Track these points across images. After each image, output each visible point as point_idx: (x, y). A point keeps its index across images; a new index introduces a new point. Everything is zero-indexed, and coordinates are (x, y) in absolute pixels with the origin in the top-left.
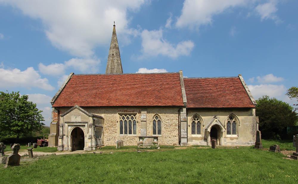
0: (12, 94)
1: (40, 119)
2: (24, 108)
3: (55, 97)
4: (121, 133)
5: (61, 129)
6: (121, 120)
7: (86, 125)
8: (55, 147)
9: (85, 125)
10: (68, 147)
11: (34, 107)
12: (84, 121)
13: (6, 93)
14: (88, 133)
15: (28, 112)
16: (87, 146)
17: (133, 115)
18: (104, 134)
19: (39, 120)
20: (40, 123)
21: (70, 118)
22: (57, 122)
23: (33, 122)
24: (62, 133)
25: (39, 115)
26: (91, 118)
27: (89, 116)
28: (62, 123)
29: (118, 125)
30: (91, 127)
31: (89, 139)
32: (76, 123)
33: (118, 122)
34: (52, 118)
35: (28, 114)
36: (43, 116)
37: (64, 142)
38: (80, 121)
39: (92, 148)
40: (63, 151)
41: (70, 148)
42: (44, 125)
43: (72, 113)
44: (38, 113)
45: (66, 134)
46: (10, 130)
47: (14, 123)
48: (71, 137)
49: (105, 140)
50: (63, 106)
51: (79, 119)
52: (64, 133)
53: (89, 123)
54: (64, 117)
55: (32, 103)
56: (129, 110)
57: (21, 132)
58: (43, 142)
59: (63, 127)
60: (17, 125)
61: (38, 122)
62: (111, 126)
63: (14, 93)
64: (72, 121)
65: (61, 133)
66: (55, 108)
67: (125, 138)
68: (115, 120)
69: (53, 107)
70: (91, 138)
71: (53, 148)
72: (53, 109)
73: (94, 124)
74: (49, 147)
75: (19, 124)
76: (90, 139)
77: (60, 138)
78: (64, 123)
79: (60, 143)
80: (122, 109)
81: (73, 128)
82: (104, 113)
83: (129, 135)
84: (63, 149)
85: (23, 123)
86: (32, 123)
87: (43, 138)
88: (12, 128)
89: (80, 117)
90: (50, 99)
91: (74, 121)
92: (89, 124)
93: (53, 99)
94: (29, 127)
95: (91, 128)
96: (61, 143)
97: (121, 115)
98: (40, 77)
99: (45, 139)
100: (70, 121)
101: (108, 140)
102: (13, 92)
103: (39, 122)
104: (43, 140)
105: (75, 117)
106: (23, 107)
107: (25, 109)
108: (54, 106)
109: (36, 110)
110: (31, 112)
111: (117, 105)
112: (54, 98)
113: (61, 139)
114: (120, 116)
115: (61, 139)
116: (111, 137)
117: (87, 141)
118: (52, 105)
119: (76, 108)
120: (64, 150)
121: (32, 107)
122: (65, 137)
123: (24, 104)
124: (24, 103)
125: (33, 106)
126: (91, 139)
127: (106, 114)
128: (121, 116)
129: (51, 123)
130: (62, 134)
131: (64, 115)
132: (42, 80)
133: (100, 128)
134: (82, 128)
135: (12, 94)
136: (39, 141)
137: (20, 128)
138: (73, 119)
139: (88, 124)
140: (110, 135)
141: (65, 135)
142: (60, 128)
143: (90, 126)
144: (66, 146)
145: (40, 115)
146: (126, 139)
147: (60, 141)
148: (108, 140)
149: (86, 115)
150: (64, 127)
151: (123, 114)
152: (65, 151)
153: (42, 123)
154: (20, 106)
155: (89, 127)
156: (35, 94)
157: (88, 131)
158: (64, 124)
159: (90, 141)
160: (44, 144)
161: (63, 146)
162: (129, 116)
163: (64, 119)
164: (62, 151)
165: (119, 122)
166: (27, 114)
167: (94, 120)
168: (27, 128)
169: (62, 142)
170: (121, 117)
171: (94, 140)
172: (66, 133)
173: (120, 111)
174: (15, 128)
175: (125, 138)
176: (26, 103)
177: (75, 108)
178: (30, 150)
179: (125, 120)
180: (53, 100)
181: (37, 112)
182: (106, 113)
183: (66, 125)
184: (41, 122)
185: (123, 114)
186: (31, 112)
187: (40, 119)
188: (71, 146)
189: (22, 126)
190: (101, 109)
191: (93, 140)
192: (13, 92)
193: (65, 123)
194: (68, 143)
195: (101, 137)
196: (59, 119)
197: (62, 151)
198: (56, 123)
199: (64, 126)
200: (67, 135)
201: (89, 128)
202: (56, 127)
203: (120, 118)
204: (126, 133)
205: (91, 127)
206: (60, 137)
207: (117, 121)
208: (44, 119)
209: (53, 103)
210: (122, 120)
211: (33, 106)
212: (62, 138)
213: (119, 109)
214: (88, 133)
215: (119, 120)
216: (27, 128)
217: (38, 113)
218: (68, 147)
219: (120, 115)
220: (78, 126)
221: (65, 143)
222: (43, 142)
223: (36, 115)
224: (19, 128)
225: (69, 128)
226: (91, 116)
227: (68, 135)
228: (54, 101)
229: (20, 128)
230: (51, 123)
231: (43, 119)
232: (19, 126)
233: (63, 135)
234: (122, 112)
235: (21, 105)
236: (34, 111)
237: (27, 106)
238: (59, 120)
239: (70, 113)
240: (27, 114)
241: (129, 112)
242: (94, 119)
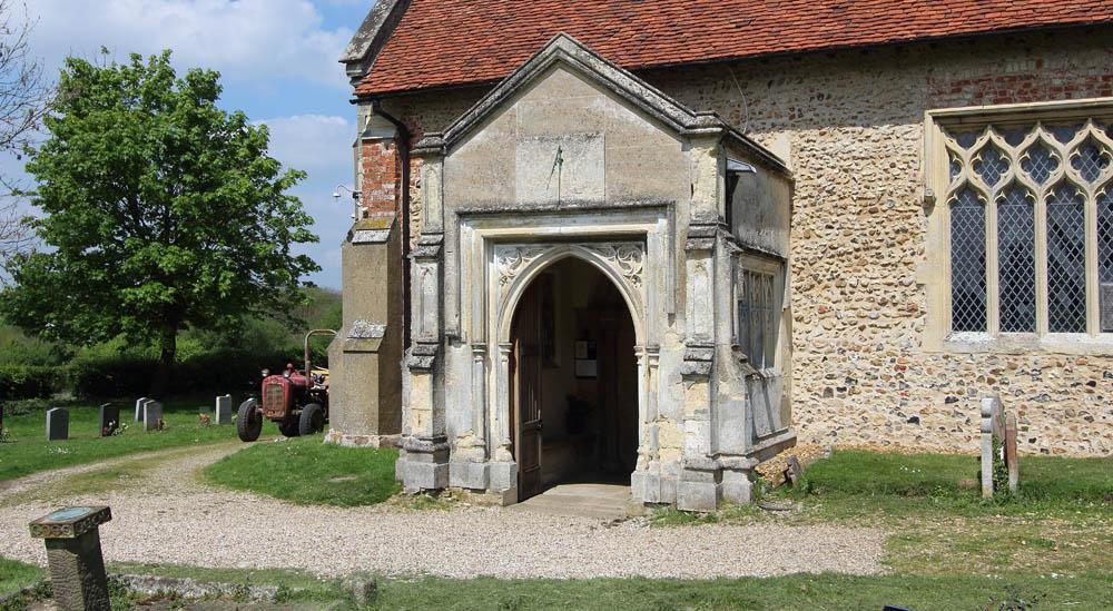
0: (131, 68)
1: (293, 230)
2: (197, 154)
3: (374, 14)
4: (967, 314)
5: (423, 278)
6: (967, 189)
7: (656, 229)
8: (376, 443)
9: (642, 237)
10: (488, 455)
11: (254, 151)
12: (637, 191)
13: (100, 63)
14: (671, 317)
15: (220, 184)
16: (669, 458)
17: (1098, 123)
18: (790, 331)
19: (285, 238)
20: (289, 259)
21: (505, 173)
22: (394, 225)
23: (250, 252)
24: (431, 317)
25: (282, 205)
26: (704, 164)
27: (689, 138)
28: (435, 217)
29: (939, 226)
30: (712, 252)
31: (689, 377)
32: (563, 212)
33: (929, 204)
34: (355, 196)
35: (220, 191)
36: (308, 208)
37: (449, 402)
38: (595, 195)
39: (718, 473)
40: (443, 498)
41: (504, 466)
42: (313, 277)
43: (519, 121)
44: (278, 187)
45: (465, 328)
46: (117, 308)
47: (140, 255)
48: (511, 356)
49: (796, 392)
50: (439, 79)
51: (587, 179)
52: (452, 321)
53: (687, 212)
54: (450, 159)
55: (241, 122)
56: (1052, 70)
57: (187, 323)
58: (299, 395)
59: (439, 258)
60: (156, 273)
61: (280, 249)
62: (865, 250)
63: (145, 63)
64: (524, 196)
65: (424, 324)
66: (376, 111)
67: (1010, 377)
68: (905, 183)
69: (362, 99)
70: (701, 373)
71: (353, 461)
72: (362, 119)
73: (728, 222)
74: (330, 446)
75: (167, 263)
76: (705, 386)
77: (416, 370)
78: (451, 224)
79: (417, 421)
80: (981, 73)
81: (529, 265)
82: (796, 120)
83: (1050, 340)
84: (442, 475)
85: (187, 254)
86: (247, 260)
87: (298, 366)
88: (128, 294)
89: (597, 147)
90: (340, 44)
91: (541, 196)
92: (683, 222)
93: (361, 30)
94: (224, 286)
95: (708, 262)
96: (428, 417)
97: (948, 124)
98: (320, 19)
99: (312, 367)
100: (505, 198)
101: (829, 392)
102: (136, 57)
103: (286, 248)
104: (297, 378)
105: (550, 160)
106: (185, 146)
107: (203, 158)
108: (364, 89)
109: (267, 164)
110: (236, 184)
111: (936, 32)
112: (366, 26)
113: (427, 379)
114: (955, 146)
115: (427, 379)
116: (859, 364)
117: (666, 403)
118: (355, 79)
119: (559, 62)
120: (455, 481)
121: (268, 182)
122: (458, 356)
123: (195, 130)
124: (193, 120)
125: (246, 142)
126: (708, 377)
127: (813, 133)
128: (966, 144)
129: (351, 235)
130: (434, 330)
131: (452, 145)
132: (327, 37)
133: (771, 266)
134: (611, 264)
135: (131, 68)
136: (276, 385)
137: (171, 290)
138: (532, 182)
139: (672, 224)
140: (852, 336)
141: (456, 339)
142: (417, 270)
143: (696, 245)
144: (465, 448)
145: (289, 204)
146: (1025, 383)
147: (417, 390)
148: (829, 392)
149: (651, 128)
150: (450, 261)
151: (981, 123)
152: (461, 497)
153: (302, 259)
154: (168, 140)
155: (690, 253)
156: (295, 118)
157: (679, 292)
158: (451, 234)
159: (703, 404)
160: (304, 412)
161: (441, 447)
162: (1050, 139)
163: (450, 186)
164: (437, 492)
165: (942, 212)
166: (211, 196)
167: (731, 179)
168: (213, 290)
169: (437, 411)
170: (966, 154)
171: (731, 387)
172: (468, 326)
173: (957, 88)
174: (140, 293)
175: (1010, 377)
176: (204, 123)
177: (549, 69)
178: (68, 545)
179: (1005, 179)
180: (358, 42)
181: (272, 182)
182: (811, 124)
183: (472, 235)
184: (295, 250)
185: (981, 123)
186: (236, 184)
187: (293, 230)
188: (511, 448)
189: (184, 275)
190: (758, 90)
191: (724, 388)
192: (136, 57)
193: (463, 216)
194: (485, 412)
195: (770, 364)
196: (407, 199)
197: (437, 492)
198: (381, 236)
199: (450, 246)
200: (478, 337)
201: (691, 263)
202: (384, 268)
203: (956, 167)
204: (1017, 317)
205: (712, 252)
206: (413, 360)
207: (921, 194)
208: (312, 230)
209: (357, 66)
210: (978, 181)
211: (246, 142)
212: (437, 370)
213: (946, 76)
214: (671, 317)
215: (942, 186)
216: (213, 290)
217: (278, 187)
218: (488, 455)
219: (951, 133)
220: (580, 252)
221: (459, 417)
222: (299, 395)
223: (266, 199)
224: (167, 295)
225: (498, 266)
226: (703, 136)
227: (485, 337)
228: (366, 46)
229: (171, 290)
230: (351, 235)
231: (306, 227)
232: (167, 280)
233: (446, 339)
234: (979, 98)
235: (179, 133)
236: (255, 174)
237: (218, 144)
238: (406, 211)
239: (502, 119)
240: (211, 196)
241: (1054, 93)
242: (732, 165)
